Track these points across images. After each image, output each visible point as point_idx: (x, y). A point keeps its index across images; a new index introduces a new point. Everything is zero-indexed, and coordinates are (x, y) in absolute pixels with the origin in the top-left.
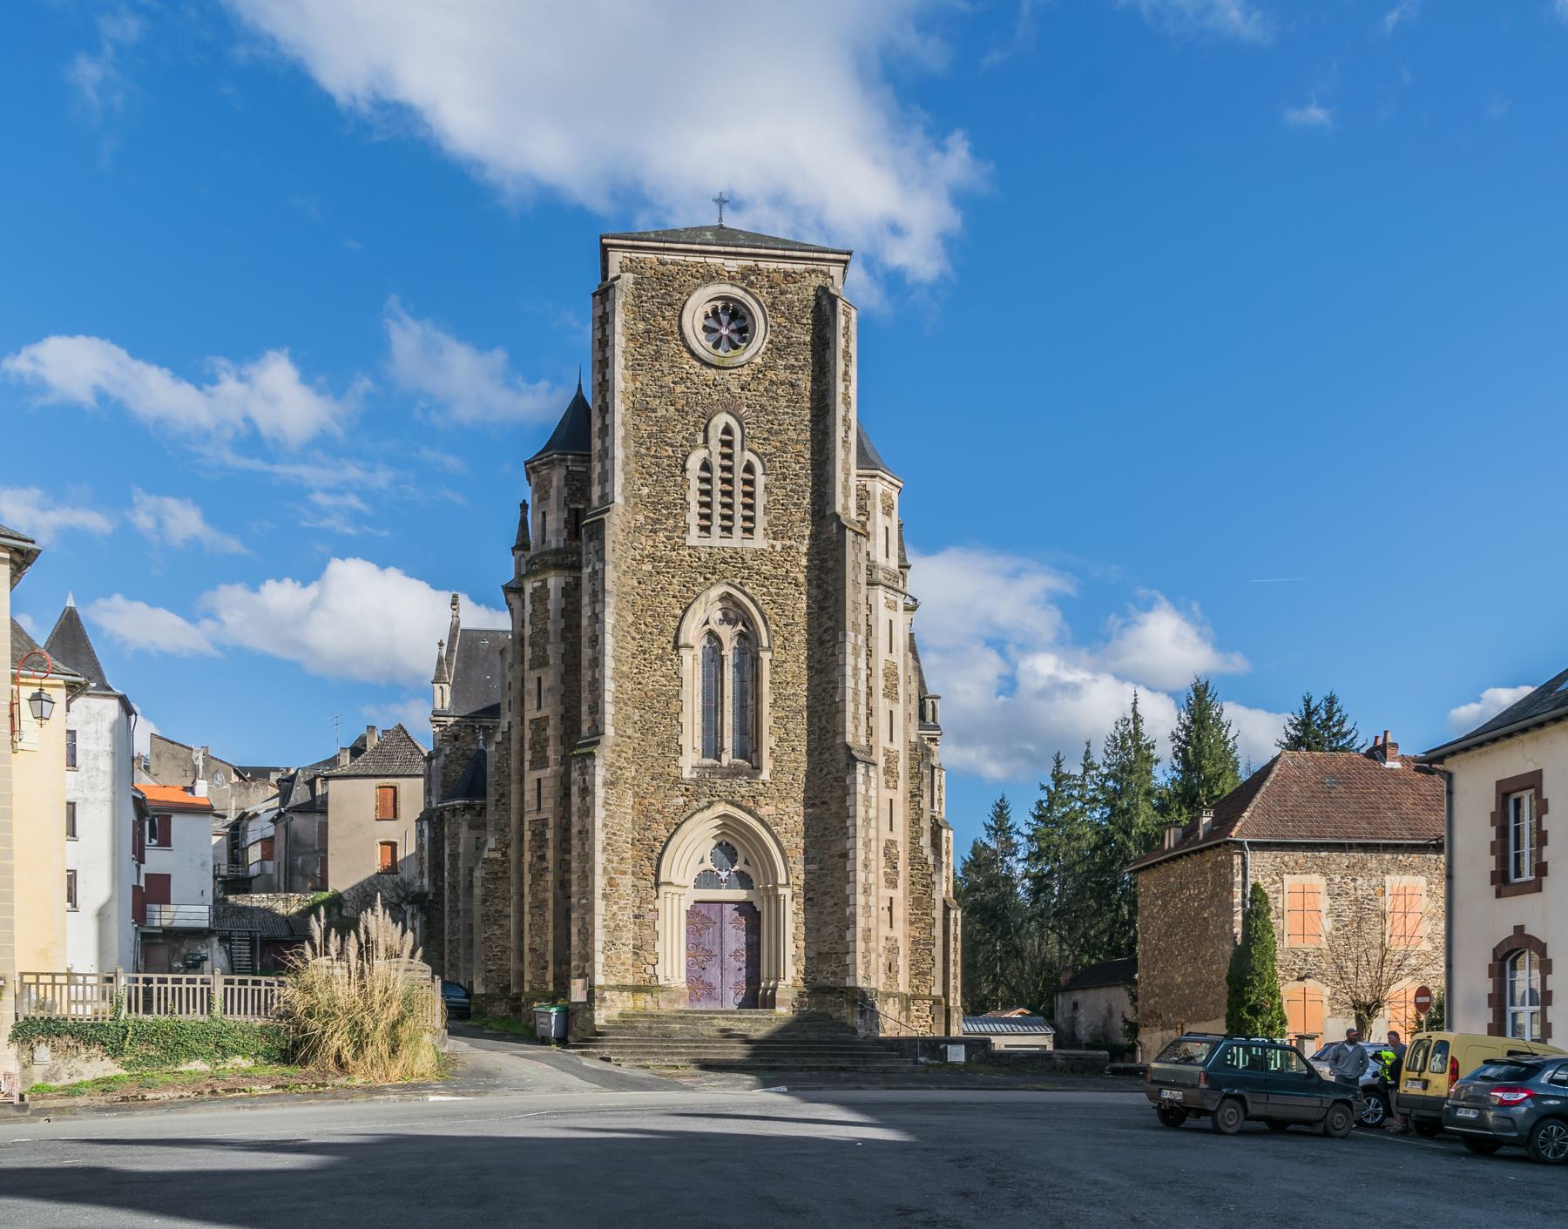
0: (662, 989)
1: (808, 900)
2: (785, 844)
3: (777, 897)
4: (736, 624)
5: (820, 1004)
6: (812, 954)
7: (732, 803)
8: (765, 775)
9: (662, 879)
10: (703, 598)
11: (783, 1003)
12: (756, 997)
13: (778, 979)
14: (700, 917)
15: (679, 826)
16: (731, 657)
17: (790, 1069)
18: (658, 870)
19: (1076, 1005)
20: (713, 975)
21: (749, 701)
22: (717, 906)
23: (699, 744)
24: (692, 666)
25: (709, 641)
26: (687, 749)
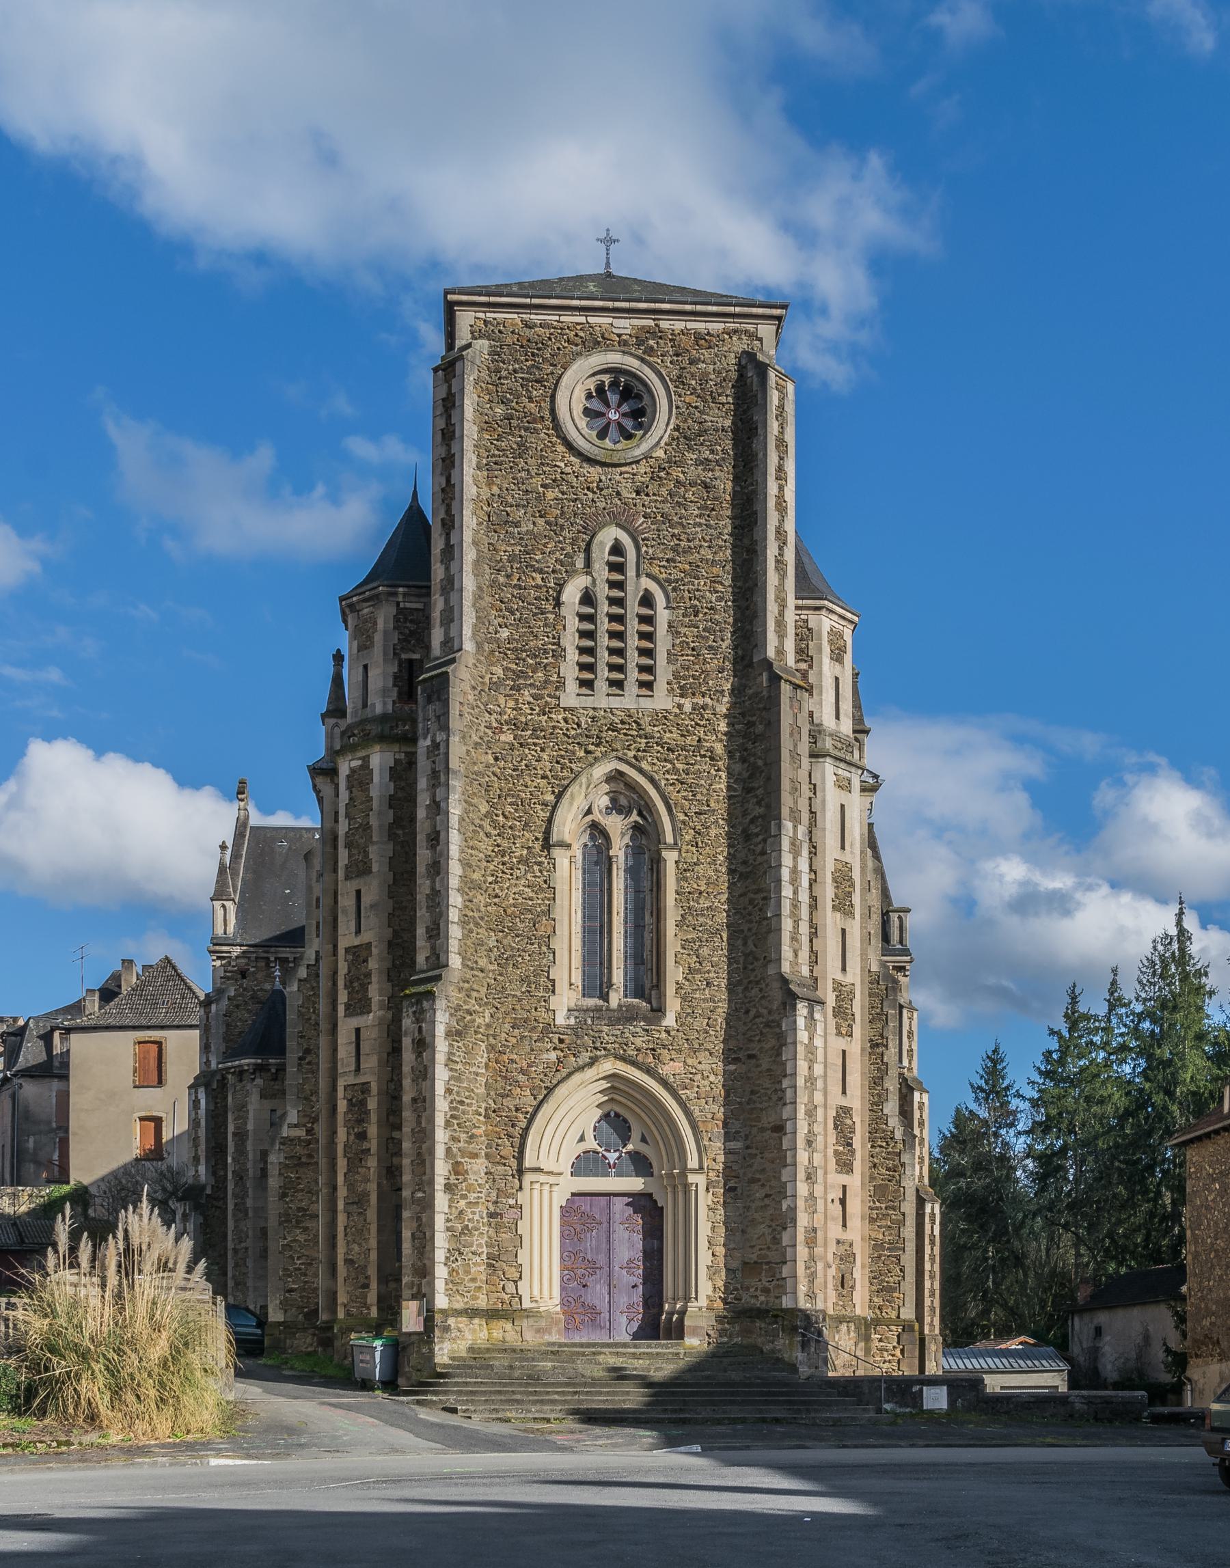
1: (729, 1190)
2: (697, 1113)
3: (686, 1186)
4: (628, 813)
5: (746, 1332)
6: (735, 1264)
7: (624, 1059)
8: (670, 1020)
9: (528, 1163)
10: (583, 779)
11: (695, 1331)
12: (657, 1324)
13: (687, 1299)
14: (579, 1216)
15: (550, 1090)
16: (621, 854)
17: (705, 1421)
20: (597, 1294)
22: (603, 1200)
23: (577, 978)
24: (568, 871)
25: (592, 837)
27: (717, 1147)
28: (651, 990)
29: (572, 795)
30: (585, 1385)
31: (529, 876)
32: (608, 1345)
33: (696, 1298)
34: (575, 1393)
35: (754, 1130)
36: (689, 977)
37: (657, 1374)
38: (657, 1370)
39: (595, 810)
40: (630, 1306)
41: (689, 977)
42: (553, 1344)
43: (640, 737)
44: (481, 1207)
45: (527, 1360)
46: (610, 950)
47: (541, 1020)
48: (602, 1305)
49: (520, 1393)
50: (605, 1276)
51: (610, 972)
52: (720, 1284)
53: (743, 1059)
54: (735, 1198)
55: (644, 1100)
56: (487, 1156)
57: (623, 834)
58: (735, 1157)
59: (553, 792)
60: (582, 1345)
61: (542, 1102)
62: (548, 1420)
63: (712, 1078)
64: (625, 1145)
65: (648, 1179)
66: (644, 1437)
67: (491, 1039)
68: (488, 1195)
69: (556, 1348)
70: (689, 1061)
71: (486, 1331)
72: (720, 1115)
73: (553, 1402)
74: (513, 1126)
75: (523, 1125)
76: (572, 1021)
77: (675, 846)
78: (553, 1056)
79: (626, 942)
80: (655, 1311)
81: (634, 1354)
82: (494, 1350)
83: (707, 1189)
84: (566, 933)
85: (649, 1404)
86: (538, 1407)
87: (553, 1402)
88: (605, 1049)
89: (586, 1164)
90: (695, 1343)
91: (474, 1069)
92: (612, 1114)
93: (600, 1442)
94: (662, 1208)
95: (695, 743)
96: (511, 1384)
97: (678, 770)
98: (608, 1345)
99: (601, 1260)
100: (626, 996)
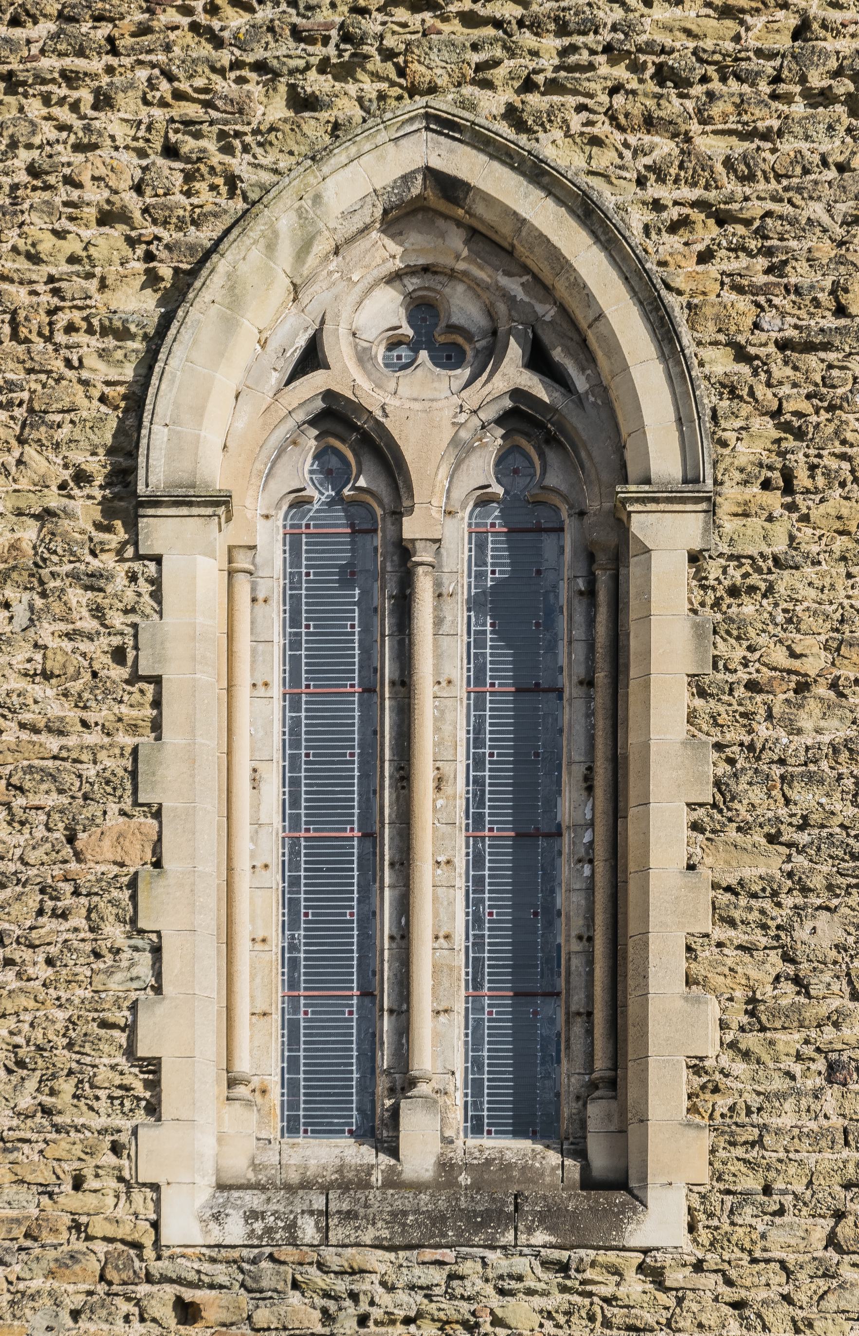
4: (490, 354)
8: (661, 1222)
10: (282, 217)
16: (456, 536)
21: (570, 805)
23: (262, 1054)
24: (221, 610)
25: (331, 469)
26: (192, 1083)
28: (582, 1099)
29: (232, 287)
31: (47, 632)
36: (751, 1041)
39: (339, 349)
41: (751, 1041)
43: (535, 26)
46: (404, 936)
47: (99, 1227)
51: (403, 1012)
57: (461, 450)
59: (152, 279)
76: (235, 1230)
77: (694, 490)
79: (474, 904)
84: (211, 867)
95: (784, 42)
97: (705, 163)
100: (477, 1127)
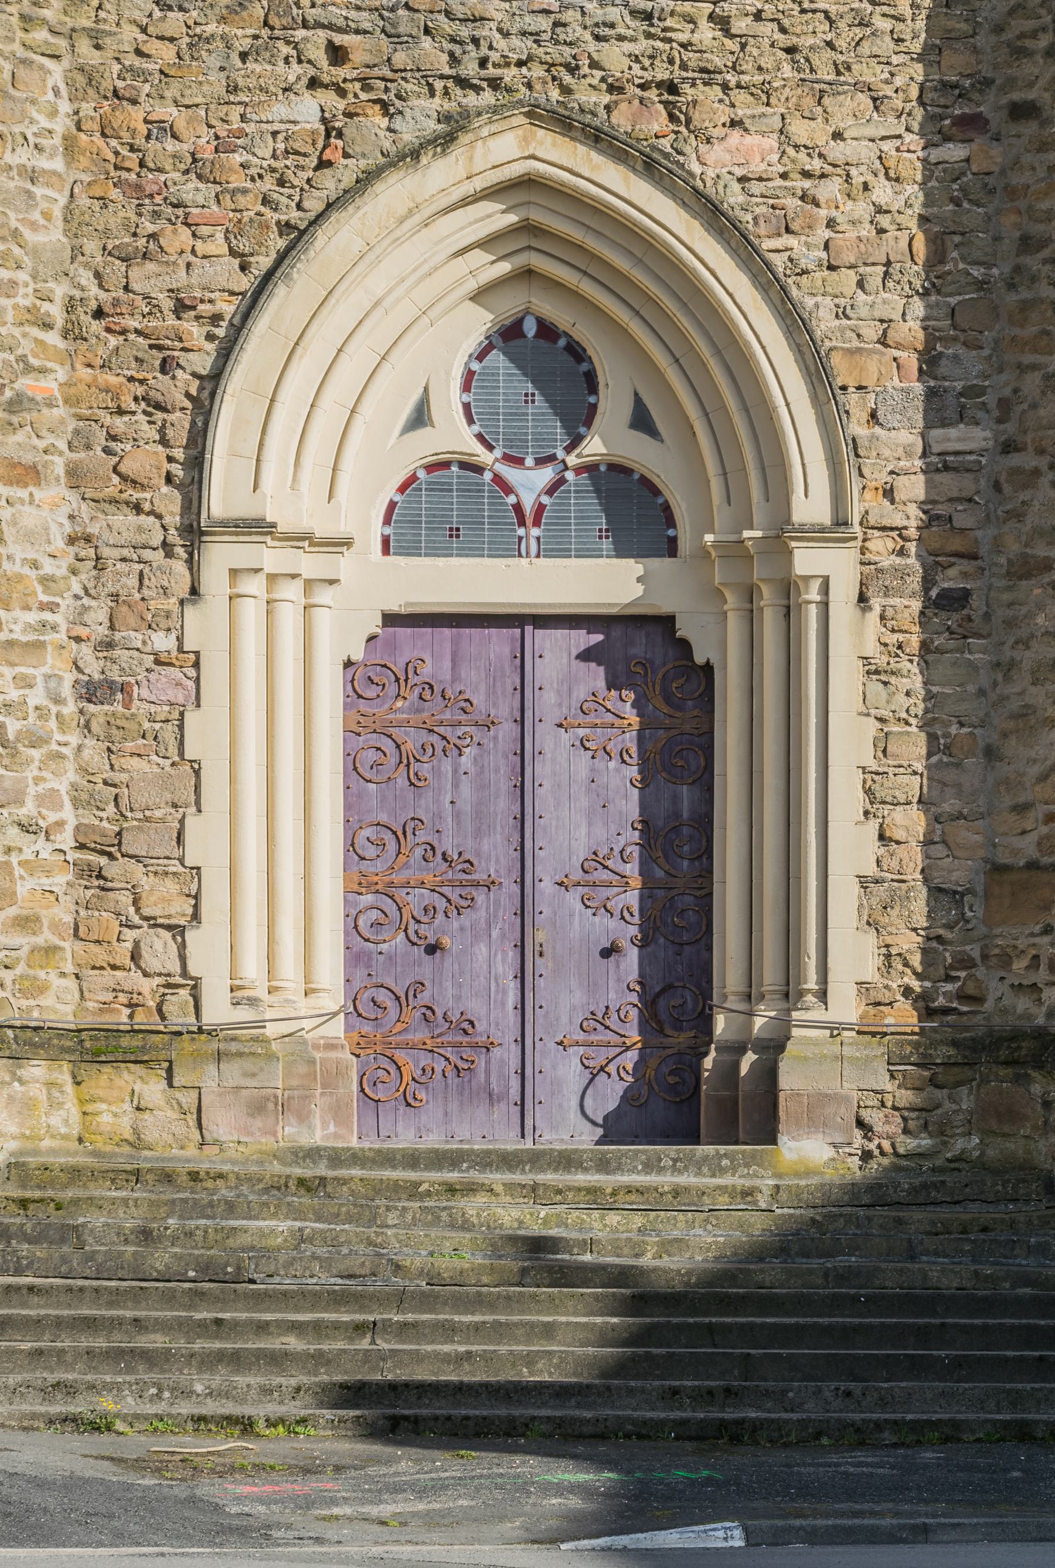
0: (221, 1045)
1: (942, 603)
2: (825, 323)
3: (789, 588)
5: (995, 1117)
6: (959, 873)
7: (563, 122)
9: (221, 500)
11: (816, 1113)
12: (690, 1088)
13: (790, 994)
14: (411, 691)
15: (298, 237)
17: (812, 1435)
18: (197, 461)
19: (208, 354)
20: (477, 976)
22: (498, 643)
27: (898, 444)
30: (401, 1299)
32: (508, 1161)
33: (823, 995)
34: (360, 1328)
35: (1032, 383)
37: (665, 1262)
38: (666, 1247)
40: (598, 1020)
42: (312, 1154)
44: (53, 663)
45: (206, 1210)
48: (497, 1019)
49: (163, 1326)
50: (507, 918)
52: (909, 943)
53: (996, 119)
54: (963, 634)
55: (638, 275)
56: (75, 476)
58: (965, 484)
60: (412, 1160)
61: (268, 277)
62: (246, 1426)
63: (883, 192)
64: (575, 442)
65: (655, 563)
66: (547, 1489)
67: (84, 46)
68: (80, 617)
69: (322, 1170)
70: (800, 130)
71: (72, 1109)
72: (911, 330)
73: (277, 1360)
74: (165, 367)
75: (203, 363)
78: (307, 110)
80: (682, 1039)
81: (593, 1191)
82: (94, 1175)
83: (862, 599)
85: (620, 1369)
86: (218, 1379)
87: (277, 1360)
88: (495, 84)
89: (438, 508)
90: (812, 1155)
91: (22, 156)
92: (530, 328)
93: (385, 1510)
94: (708, 669)
96: (137, 1297)
98: (508, 1161)
99: (495, 856)
